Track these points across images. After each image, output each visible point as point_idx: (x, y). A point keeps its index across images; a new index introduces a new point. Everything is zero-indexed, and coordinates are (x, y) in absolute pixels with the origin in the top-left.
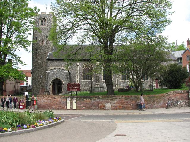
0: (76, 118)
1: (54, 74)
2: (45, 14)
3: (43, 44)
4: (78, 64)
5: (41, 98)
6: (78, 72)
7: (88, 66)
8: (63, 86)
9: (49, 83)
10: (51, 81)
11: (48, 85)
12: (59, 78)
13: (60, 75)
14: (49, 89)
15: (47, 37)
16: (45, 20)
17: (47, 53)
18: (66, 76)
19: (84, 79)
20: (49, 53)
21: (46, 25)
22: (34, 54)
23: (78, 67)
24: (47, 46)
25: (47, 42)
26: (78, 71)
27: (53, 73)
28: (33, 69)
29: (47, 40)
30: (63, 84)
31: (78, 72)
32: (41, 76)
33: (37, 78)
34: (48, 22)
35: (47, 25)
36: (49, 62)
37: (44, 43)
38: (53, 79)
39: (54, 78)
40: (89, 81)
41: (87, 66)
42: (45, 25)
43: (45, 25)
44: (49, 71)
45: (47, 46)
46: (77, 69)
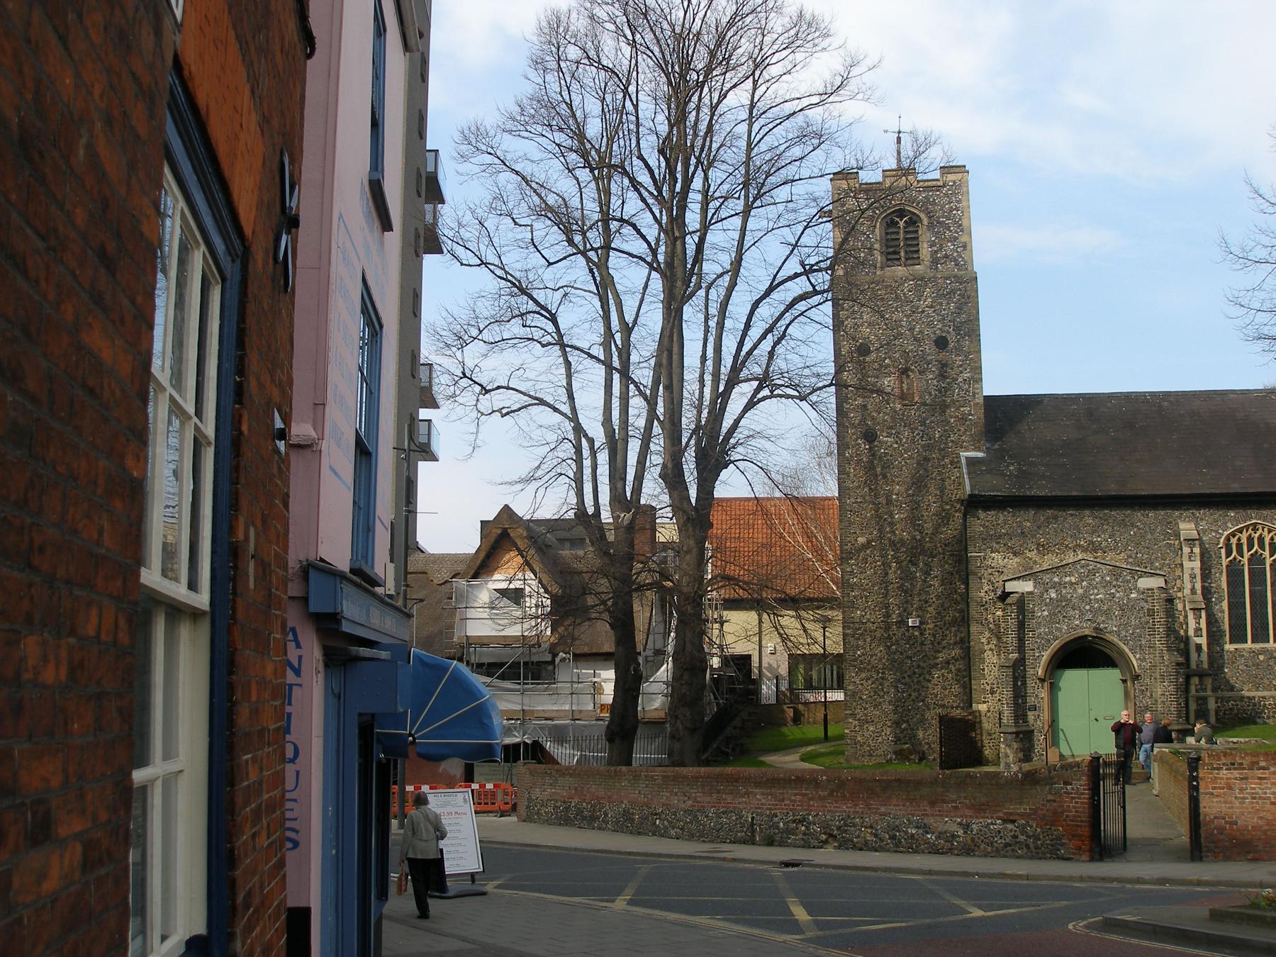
0: (696, 778)
1: (1061, 606)
4: (1187, 528)
5: (1236, 773)
6: (1193, 591)
7: (1261, 539)
9: (1030, 672)
10: (1046, 655)
13: (1107, 613)
16: (913, 222)
23: (1197, 550)
26: (1193, 577)
31: (1198, 586)
36: (983, 521)
38: (1056, 644)
41: (1250, 539)
43: (913, 256)
46: (1187, 564)
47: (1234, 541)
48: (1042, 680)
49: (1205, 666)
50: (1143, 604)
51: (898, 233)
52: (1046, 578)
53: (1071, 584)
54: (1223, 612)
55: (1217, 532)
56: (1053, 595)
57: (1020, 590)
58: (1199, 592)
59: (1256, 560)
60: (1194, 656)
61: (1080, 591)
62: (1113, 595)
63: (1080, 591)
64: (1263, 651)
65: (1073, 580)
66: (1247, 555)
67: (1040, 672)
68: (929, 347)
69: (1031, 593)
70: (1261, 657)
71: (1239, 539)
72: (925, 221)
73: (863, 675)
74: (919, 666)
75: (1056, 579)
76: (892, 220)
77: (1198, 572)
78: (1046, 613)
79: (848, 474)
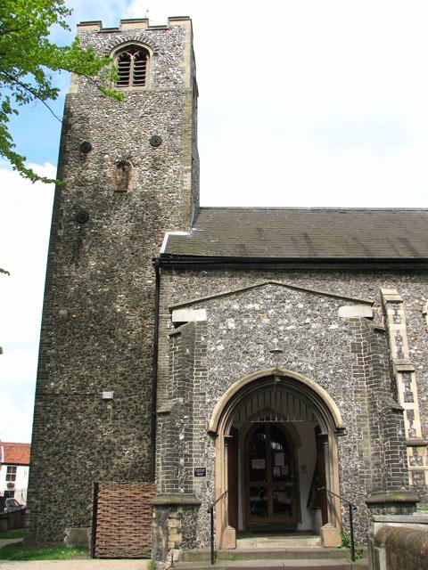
1: (240, 340)
2: (143, 26)
8: (335, 446)
10: (220, 401)
11: (189, 438)
12: (296, 375)
14: (197, 483)
15: (156, 142)
16: (143, 55)
17: (153, 235)
18: (355, 348)
25: (155, 168)
26: (399, 339)
27: (231, 324)
30: (339, 431)
32: (107, 395)
33: (73, 412)
35: (156, 80)
37: (135, 172)
38: (234, 387)
39: (245, 372)
43: (140, 80)
48: (213, 435)
49: (419, 434)
50: (347, 337)
51: (129, 65)
53: (255, 311)
55: (419, 299)
57: (189, 320)
58: (406, 356)
61: (266, 321)
63: (266, 321)
65: (257, 307)
67: (212, 424)
68: (145, 146)
69: (204, 323)
72: (151, 54)
73: (51, 450)
74: (109, 441)
75: (236, 307)
76: (125, 54)
77: (403, 334)
78: (221, 348)
79: (58, 251)
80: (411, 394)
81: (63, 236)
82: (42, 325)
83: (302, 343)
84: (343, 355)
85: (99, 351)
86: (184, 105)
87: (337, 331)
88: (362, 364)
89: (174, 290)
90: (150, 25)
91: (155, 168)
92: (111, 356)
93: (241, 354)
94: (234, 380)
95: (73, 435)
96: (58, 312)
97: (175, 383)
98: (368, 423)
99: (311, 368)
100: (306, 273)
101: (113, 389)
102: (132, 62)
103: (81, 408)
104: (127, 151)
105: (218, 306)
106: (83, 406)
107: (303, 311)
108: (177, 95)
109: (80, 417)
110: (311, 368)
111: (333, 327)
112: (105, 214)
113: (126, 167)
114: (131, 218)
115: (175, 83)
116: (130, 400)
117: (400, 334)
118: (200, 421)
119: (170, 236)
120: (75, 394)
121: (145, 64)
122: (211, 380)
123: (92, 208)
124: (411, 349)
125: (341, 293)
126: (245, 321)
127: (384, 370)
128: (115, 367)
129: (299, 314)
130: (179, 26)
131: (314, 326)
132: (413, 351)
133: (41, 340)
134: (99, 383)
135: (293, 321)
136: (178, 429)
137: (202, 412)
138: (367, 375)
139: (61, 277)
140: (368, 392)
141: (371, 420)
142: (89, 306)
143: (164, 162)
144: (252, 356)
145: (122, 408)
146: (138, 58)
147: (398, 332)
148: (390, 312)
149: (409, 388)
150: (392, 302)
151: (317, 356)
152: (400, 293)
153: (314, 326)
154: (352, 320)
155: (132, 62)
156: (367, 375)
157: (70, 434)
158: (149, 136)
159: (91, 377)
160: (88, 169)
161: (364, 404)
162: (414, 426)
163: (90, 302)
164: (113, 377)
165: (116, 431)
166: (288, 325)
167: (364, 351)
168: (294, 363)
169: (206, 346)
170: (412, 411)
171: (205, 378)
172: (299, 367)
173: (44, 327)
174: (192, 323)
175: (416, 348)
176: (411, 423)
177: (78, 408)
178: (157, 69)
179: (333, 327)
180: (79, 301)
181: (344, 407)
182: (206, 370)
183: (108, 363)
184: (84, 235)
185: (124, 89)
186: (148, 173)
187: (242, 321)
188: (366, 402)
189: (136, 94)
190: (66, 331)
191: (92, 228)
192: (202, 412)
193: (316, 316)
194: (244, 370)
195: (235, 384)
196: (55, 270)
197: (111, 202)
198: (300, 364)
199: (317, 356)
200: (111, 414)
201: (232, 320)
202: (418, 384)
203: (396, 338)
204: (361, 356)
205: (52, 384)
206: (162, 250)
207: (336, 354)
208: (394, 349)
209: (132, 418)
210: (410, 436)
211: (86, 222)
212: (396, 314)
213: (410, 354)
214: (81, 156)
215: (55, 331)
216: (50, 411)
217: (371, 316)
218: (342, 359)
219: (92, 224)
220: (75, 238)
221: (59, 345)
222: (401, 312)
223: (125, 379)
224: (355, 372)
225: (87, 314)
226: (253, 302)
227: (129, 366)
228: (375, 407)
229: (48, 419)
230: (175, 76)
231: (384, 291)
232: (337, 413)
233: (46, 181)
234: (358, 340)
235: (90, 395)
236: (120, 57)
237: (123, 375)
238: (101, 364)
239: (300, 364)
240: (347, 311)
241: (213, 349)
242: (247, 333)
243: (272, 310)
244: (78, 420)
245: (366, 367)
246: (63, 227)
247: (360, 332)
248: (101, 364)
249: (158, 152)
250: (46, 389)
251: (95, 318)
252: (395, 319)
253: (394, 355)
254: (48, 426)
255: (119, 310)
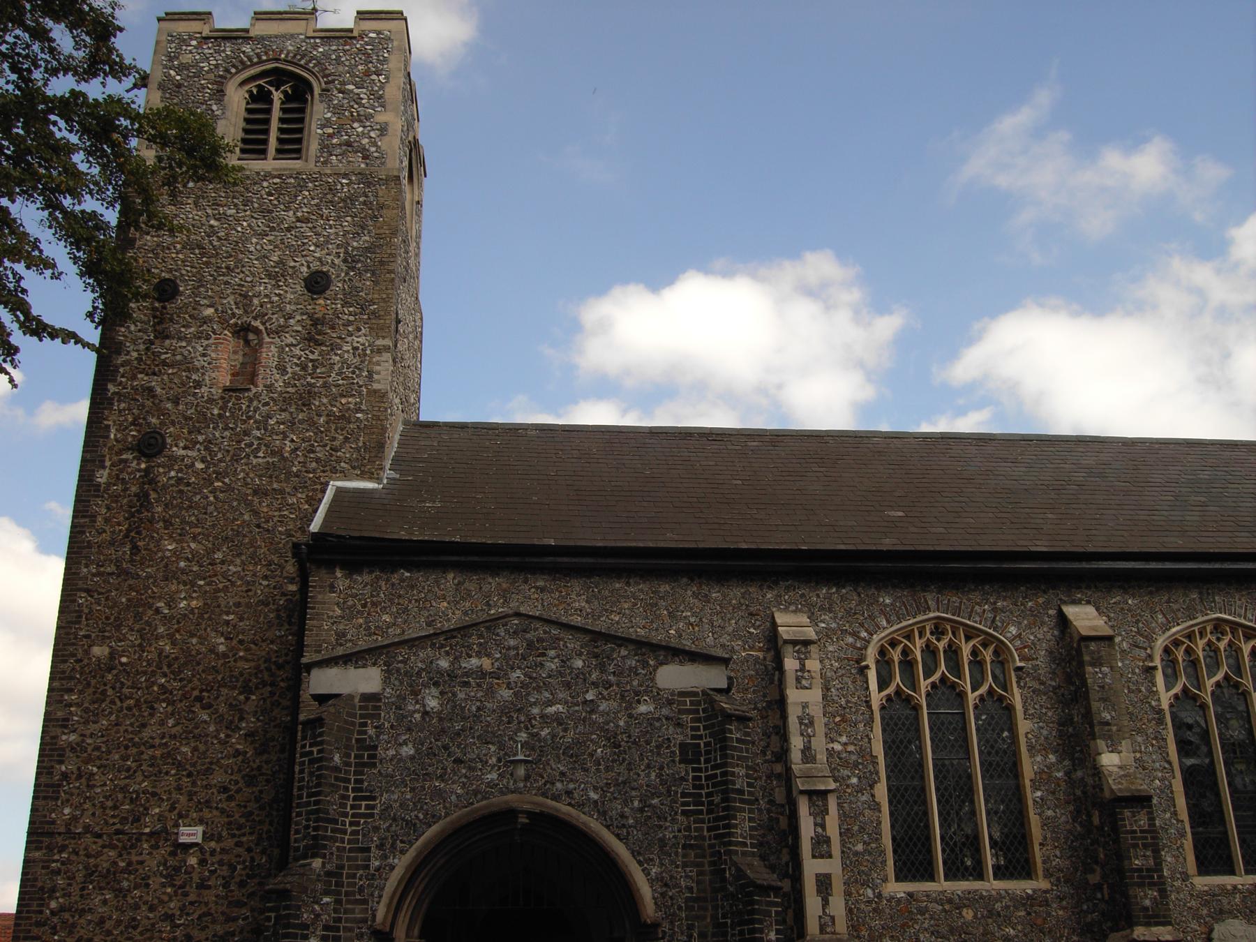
3: (248, 372)
7: (953, 653)
10: (401, 863)
15: (317, 284)
16: (300, 93)
19: (914, 863)
20: (334, 485)
21: (313, 147)
22: (100, 508)
24: (305, 398)
25: (311, 340)
28: (64, 724)
29: (316, 322)
34: (338, 110)
35: (326, 148)
37: (270, 354)
39: (456, 799)
40: (942, 885)
41: (930, 650)
42: (297, 153)
43: (292, 145)
44: (365, 680)
45: (305, 398)
47: (896, 655)
52: (417, 662)
53: (482, 674)
54: (877, 807)
55: (855, 634)
56: (432, 703)
58: (822, 757)
59: (947, 691)
60: (812, 903)
61: (506, 694)
62: (592, 706)
63: (506, 694)
64: (971, 900)
65: (486, 663)
66: (924, 685)
68: (294, 291)
70: (968, 914)
71: (905, 652)
72: (317, 91)
75: (444, 664)
77: (816, 711)
78: (408, 750)
79: (93, 518)
80: (828, 841)
81: (108, 484)
82: (52, 679)
83: (577, 743)
84: (661, 768)
85: (173, 737)
86: (381, 207)
87: (650, 720)
88: (701, 787)
89: (338, 612)
90: (319, 26)
91: (311, 340)
92: (202, 747)
93: (450, 765)
94: (436, 818)
95: (109, 925)
96: (87, 652)
97: (307, 827)
98: (709, 914)
99: (594, 796)
100: (619, 577)
101: (201, 821)
102: (277, 105)
103: (130, 864)
104: (256, 301)
105: (404, 662)
106: (134, 858)
107: (582, 675)
108: (369, 184)
109: (125, 884)
110: (594, 796)
111: (643, 708)
112: (200, 438)
113: (251, 336)
114: (258, 449)
115: (365, 157)
116: (238, 844)
117: (810, 711)
118: (358, 907)
119: (339, 491)
120: (118, 832)
121: (302, 110)
122: (385, 820)
123: (173, 423)
124: (832, 741)
125: (670, 633)
126: (461, 696)
127: (743, 801)
128: (209, 771)
129: (572, 681)
130: (379, 33)
131: (603, 706)
132: (838, 747)
133: (47, 714)
134: (172, 809)
135: (561, 696)
136: (306, 927)
137: (361, 890)
138: (710, 812)
139: (98, 574)
140: (711, 846)
141: (716, 908)
142: (157, 638)
143: (333, 328)
144: (471, 769)
145: (221, 863)
146: (288, 98)
147: (805, 706)
148: (790, 664)
149: (823, 826)
150: (794, 643)
151: (607, 769)
152: (814, 621)
153: (603, 706)
154: (683, 694)
155: (277, 105)
156: (710, 812)
157: (102, 921)
158: (315, 266)
159: (154, 794)
160: (167, 337)
161: (700, 873)
162: (831, 910)
163: (161, 630)
164: (202, 796)
165: (204, 915)
166: (550, 703)
167: (707, 761)
168: (559, 785)
169: (375, 748)
170: (828, 877)
171: (372, 815)
172: (569, 793)
173: (56, 684)
174: (351, 697)
175: (844, 739)
176: (826, 903)
177: (122, 864)
178: (327, 123)
179: (643, 708)
180: (137, 627)
181: (659, 878)
182: (374, 799)
183: (194, 765)
184: (152, 482)
185: (255, 165)
186: (297, 351)
187: (454, 695)
188: (707, 868)
189: (279, 177)
190: (104, 693)
191: (171, 468)
192: (361, 890)
193: (608, 685)
194: (453, 798)
195: (435, 828)
196: (87, 558)
197: (216, 412)
198: (571, 786)
199: (607, 769)
200: (196, 879)
201: (435, 691)
202: (843, 817)
203: (800, 719)
204: (700, 770)
205: (67, 811)
206: (315, 526)
207: (648, 766)
208: (796, 743)
209: (242, 884)
210: (822, 929)
211: (160, 452)
212: (802, 668)
213: (831, 753)
214: (154, 309)
215: (81, 692)
216: (60, 870)
217: (723, 684)
218: (659, 776)
219: (173, 459)
220: (134, 489)
221: (86, 722)
222: (813, 665)
223: (230, 798)
224: (684, 804)
225: (154, 656)
226: (479, 655)
227: (239, 771)
228: (724, 880)
229: (53, 890)
230: (365, 141)
231: (780, 618)
232: (645, 890)
233: (86, 345)
234: (693, 737)
235: (151, 834)
236: (250, 92)
237: (225, 789)
238: (179, 766)
239: (571, 786)
240: (673, 677)
241: (391, 752)
242: (464, 718)
243: (518, 673)
244: (120, 890)
245: (709, 795)
246: (108, 464)
247: (699, 720)
248: (179, 766)
249: (321, 305)
250: (53, 822)
251: (169, 666)
252: (798, 680)
253: (796, 755)
254: (53, 904)
255: (222, 648)
